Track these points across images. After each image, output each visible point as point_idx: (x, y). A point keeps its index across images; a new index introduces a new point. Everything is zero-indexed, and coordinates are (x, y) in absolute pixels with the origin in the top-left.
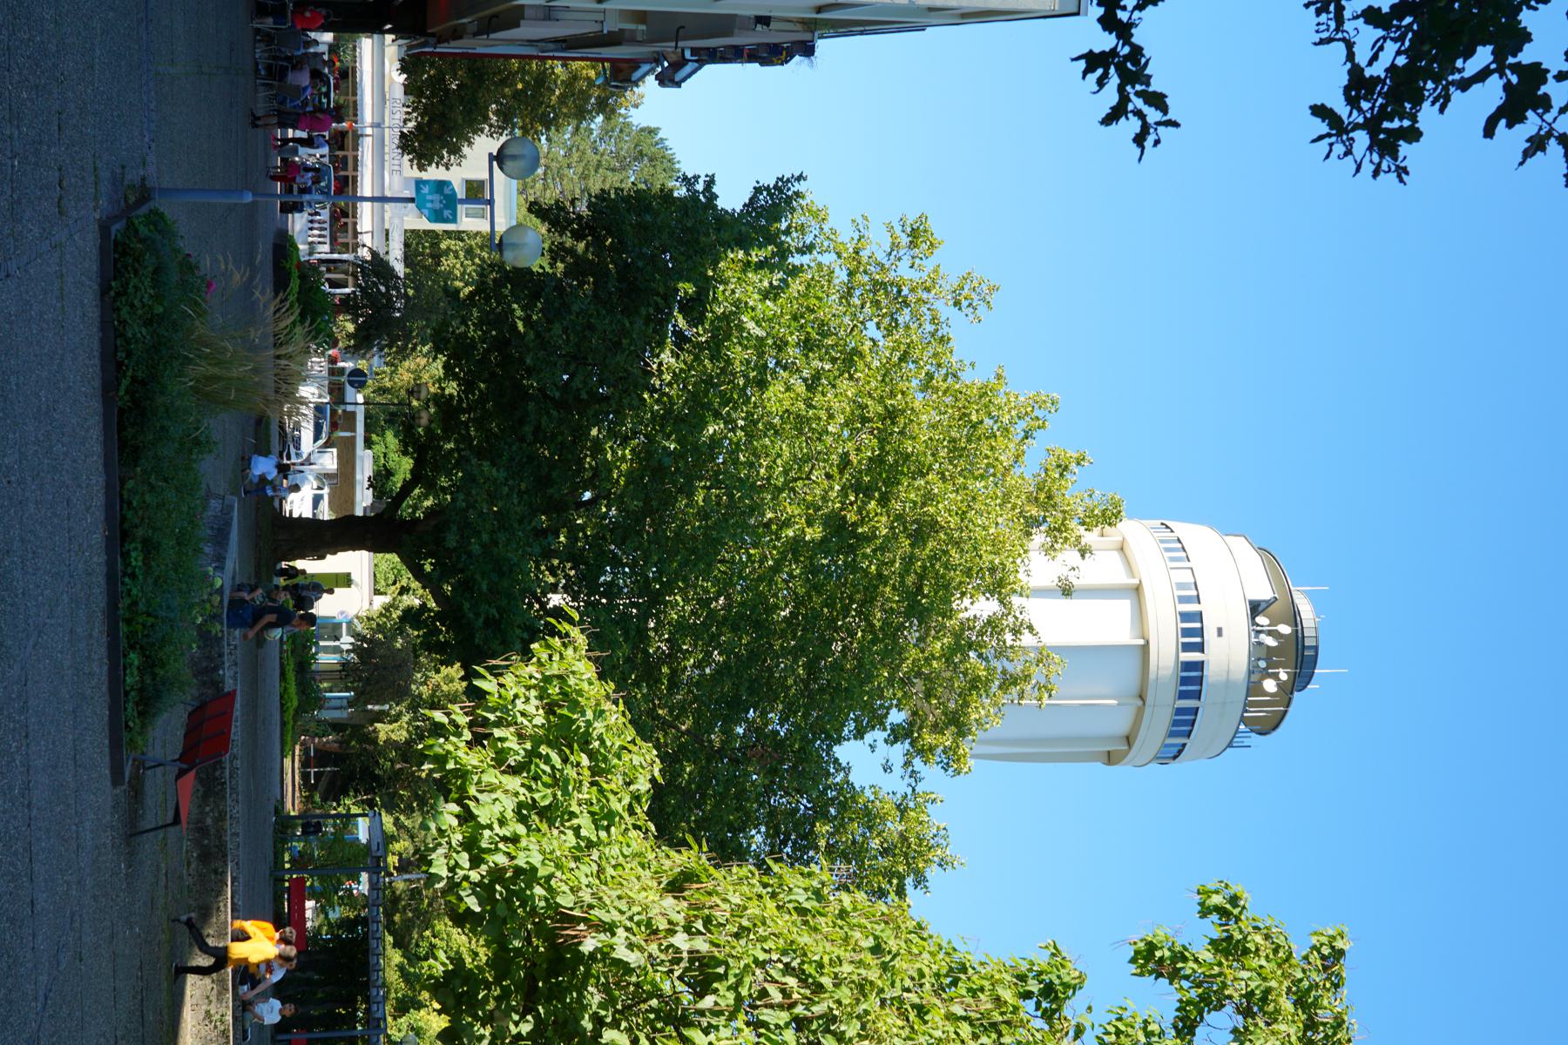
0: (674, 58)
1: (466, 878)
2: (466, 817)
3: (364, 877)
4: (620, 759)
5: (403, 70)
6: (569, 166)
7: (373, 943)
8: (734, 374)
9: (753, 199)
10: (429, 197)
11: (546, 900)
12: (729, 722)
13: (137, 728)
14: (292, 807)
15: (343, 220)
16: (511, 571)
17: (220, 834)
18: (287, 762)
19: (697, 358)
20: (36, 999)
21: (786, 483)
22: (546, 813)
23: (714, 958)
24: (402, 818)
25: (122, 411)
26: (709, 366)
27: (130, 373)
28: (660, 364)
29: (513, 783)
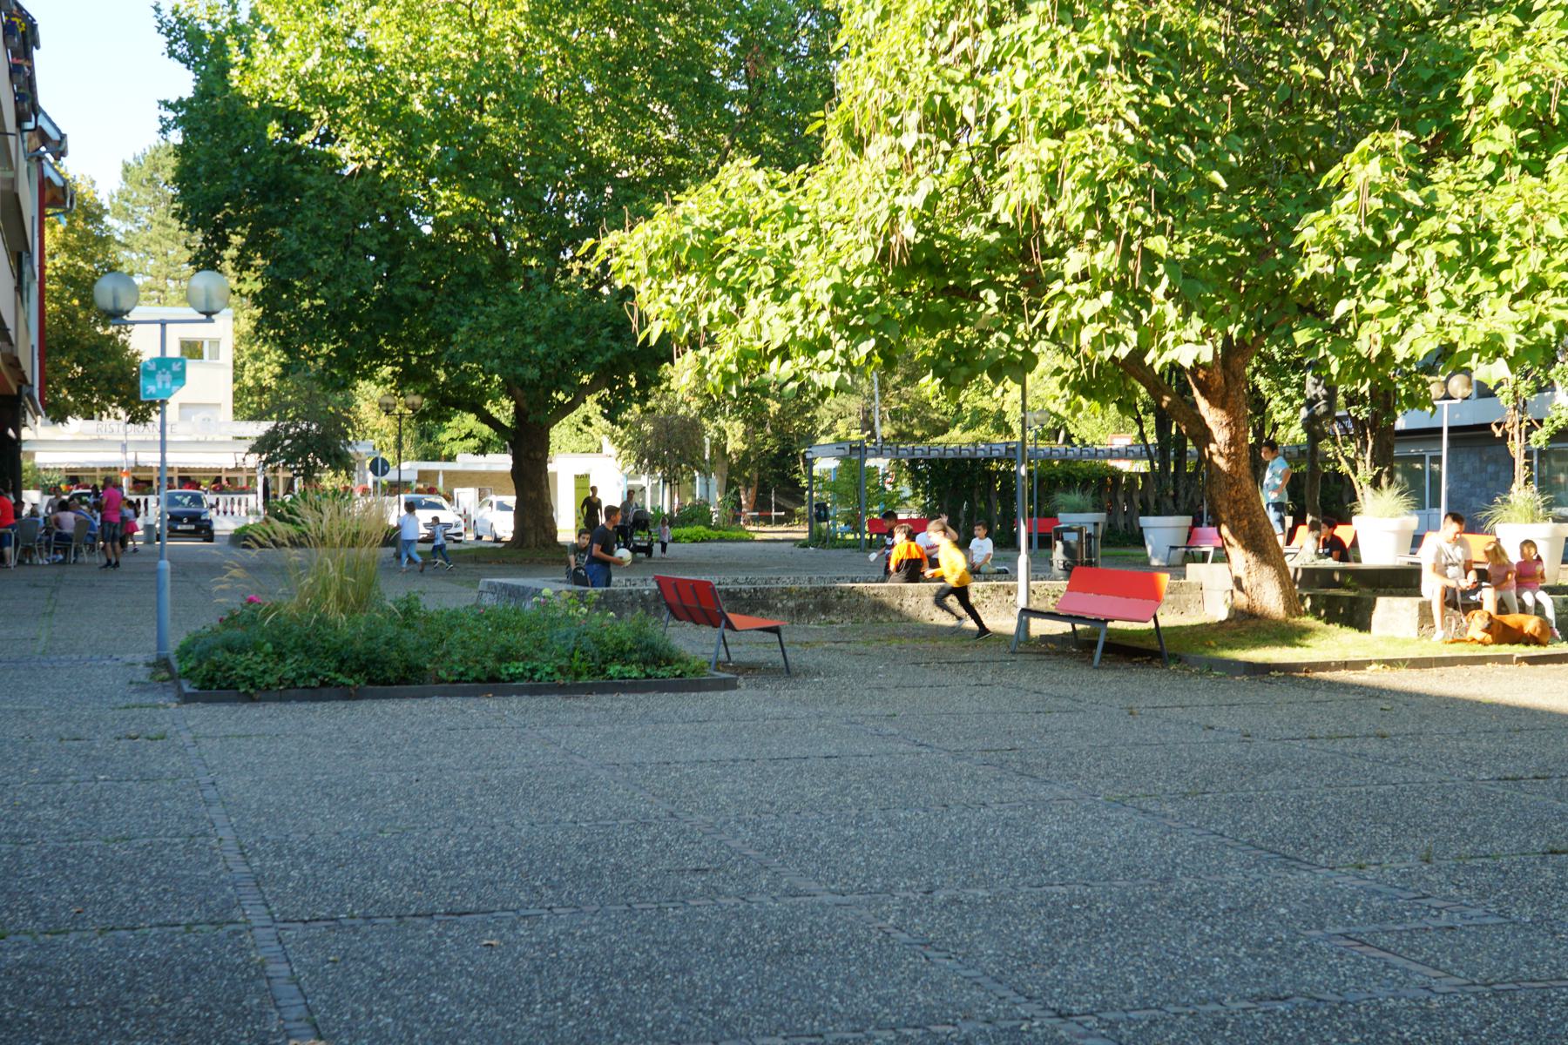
0: (36, 141)
1: (844, 354)
2: (784, 353)
3: (870, 462)
4: (732, 200)
5: (63, 420)
6: (166, 254)
7: (934, 454)
8: (361, 83)
9: (182, 60)
10: (160, 385)
11: (867, 275)
12: (721, 96)
13: (683, 666)
14: (801, 532)
15: (224, 482)
16: (565, 314)
17: (802, 594)
18: (758, 536)
19: (345, 120)
20: (919, 754)
21: (476, 30)
22: (781, 274)
23: (926, 107)
24: (821, 428)
25: (371, 682)
26: (353, 108)
27: (332, 674)
28: (353, 159)
29: (752, 306)
